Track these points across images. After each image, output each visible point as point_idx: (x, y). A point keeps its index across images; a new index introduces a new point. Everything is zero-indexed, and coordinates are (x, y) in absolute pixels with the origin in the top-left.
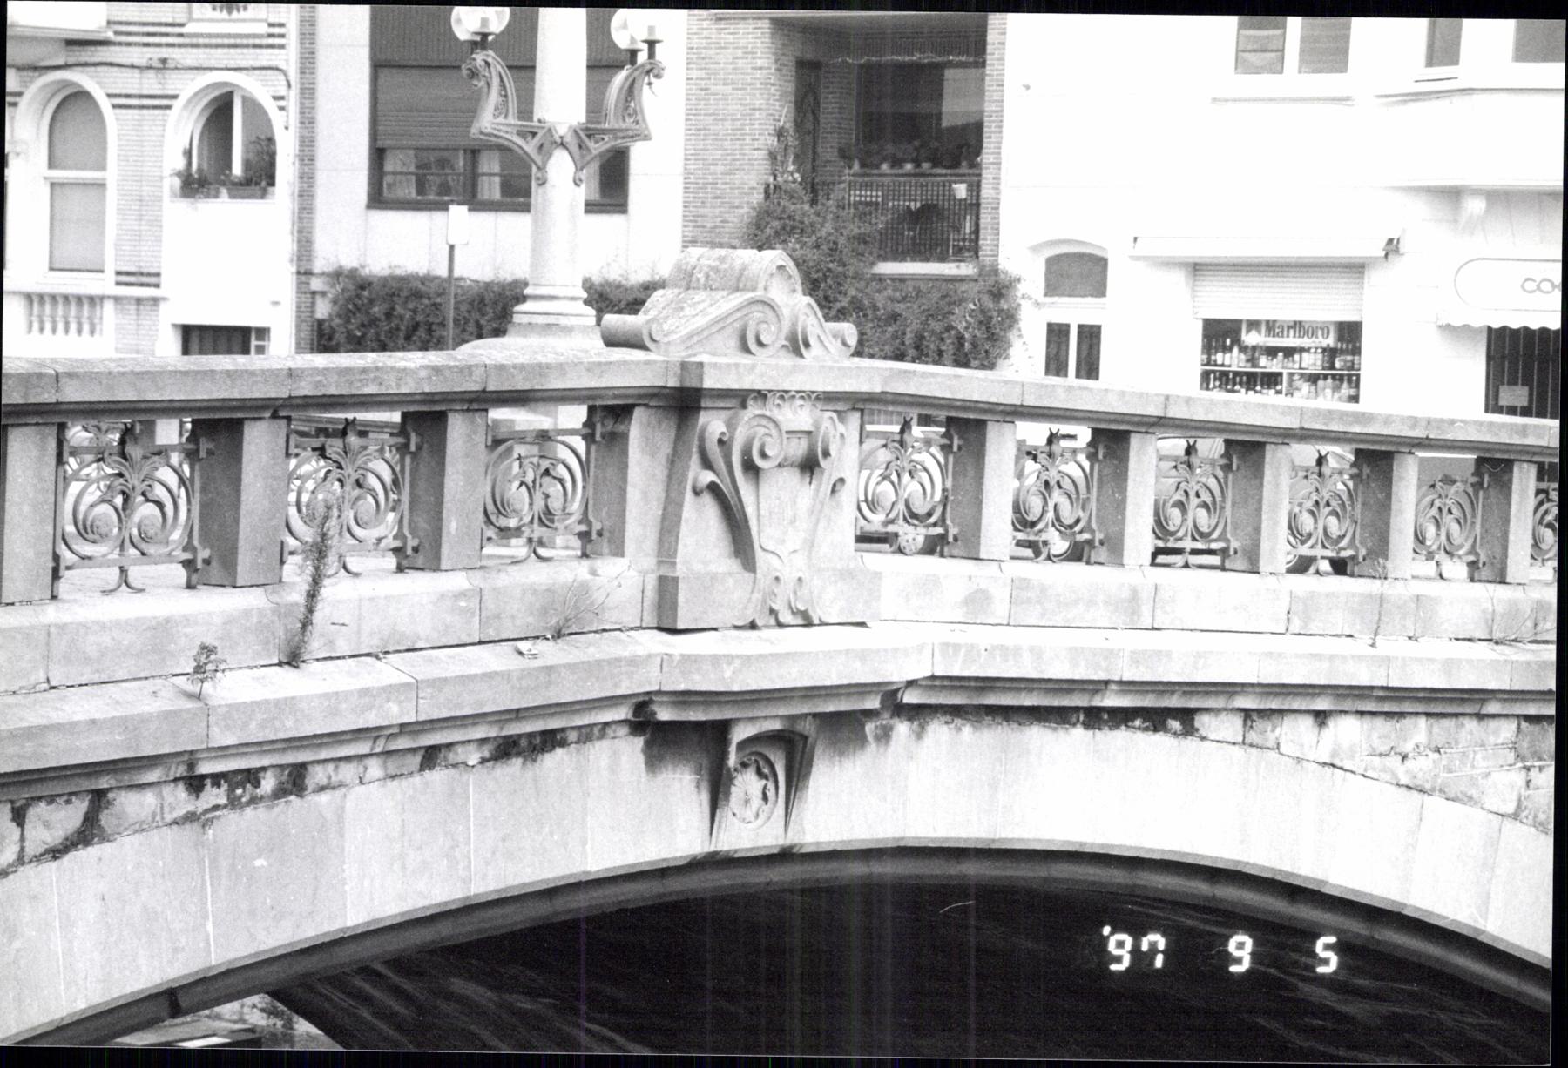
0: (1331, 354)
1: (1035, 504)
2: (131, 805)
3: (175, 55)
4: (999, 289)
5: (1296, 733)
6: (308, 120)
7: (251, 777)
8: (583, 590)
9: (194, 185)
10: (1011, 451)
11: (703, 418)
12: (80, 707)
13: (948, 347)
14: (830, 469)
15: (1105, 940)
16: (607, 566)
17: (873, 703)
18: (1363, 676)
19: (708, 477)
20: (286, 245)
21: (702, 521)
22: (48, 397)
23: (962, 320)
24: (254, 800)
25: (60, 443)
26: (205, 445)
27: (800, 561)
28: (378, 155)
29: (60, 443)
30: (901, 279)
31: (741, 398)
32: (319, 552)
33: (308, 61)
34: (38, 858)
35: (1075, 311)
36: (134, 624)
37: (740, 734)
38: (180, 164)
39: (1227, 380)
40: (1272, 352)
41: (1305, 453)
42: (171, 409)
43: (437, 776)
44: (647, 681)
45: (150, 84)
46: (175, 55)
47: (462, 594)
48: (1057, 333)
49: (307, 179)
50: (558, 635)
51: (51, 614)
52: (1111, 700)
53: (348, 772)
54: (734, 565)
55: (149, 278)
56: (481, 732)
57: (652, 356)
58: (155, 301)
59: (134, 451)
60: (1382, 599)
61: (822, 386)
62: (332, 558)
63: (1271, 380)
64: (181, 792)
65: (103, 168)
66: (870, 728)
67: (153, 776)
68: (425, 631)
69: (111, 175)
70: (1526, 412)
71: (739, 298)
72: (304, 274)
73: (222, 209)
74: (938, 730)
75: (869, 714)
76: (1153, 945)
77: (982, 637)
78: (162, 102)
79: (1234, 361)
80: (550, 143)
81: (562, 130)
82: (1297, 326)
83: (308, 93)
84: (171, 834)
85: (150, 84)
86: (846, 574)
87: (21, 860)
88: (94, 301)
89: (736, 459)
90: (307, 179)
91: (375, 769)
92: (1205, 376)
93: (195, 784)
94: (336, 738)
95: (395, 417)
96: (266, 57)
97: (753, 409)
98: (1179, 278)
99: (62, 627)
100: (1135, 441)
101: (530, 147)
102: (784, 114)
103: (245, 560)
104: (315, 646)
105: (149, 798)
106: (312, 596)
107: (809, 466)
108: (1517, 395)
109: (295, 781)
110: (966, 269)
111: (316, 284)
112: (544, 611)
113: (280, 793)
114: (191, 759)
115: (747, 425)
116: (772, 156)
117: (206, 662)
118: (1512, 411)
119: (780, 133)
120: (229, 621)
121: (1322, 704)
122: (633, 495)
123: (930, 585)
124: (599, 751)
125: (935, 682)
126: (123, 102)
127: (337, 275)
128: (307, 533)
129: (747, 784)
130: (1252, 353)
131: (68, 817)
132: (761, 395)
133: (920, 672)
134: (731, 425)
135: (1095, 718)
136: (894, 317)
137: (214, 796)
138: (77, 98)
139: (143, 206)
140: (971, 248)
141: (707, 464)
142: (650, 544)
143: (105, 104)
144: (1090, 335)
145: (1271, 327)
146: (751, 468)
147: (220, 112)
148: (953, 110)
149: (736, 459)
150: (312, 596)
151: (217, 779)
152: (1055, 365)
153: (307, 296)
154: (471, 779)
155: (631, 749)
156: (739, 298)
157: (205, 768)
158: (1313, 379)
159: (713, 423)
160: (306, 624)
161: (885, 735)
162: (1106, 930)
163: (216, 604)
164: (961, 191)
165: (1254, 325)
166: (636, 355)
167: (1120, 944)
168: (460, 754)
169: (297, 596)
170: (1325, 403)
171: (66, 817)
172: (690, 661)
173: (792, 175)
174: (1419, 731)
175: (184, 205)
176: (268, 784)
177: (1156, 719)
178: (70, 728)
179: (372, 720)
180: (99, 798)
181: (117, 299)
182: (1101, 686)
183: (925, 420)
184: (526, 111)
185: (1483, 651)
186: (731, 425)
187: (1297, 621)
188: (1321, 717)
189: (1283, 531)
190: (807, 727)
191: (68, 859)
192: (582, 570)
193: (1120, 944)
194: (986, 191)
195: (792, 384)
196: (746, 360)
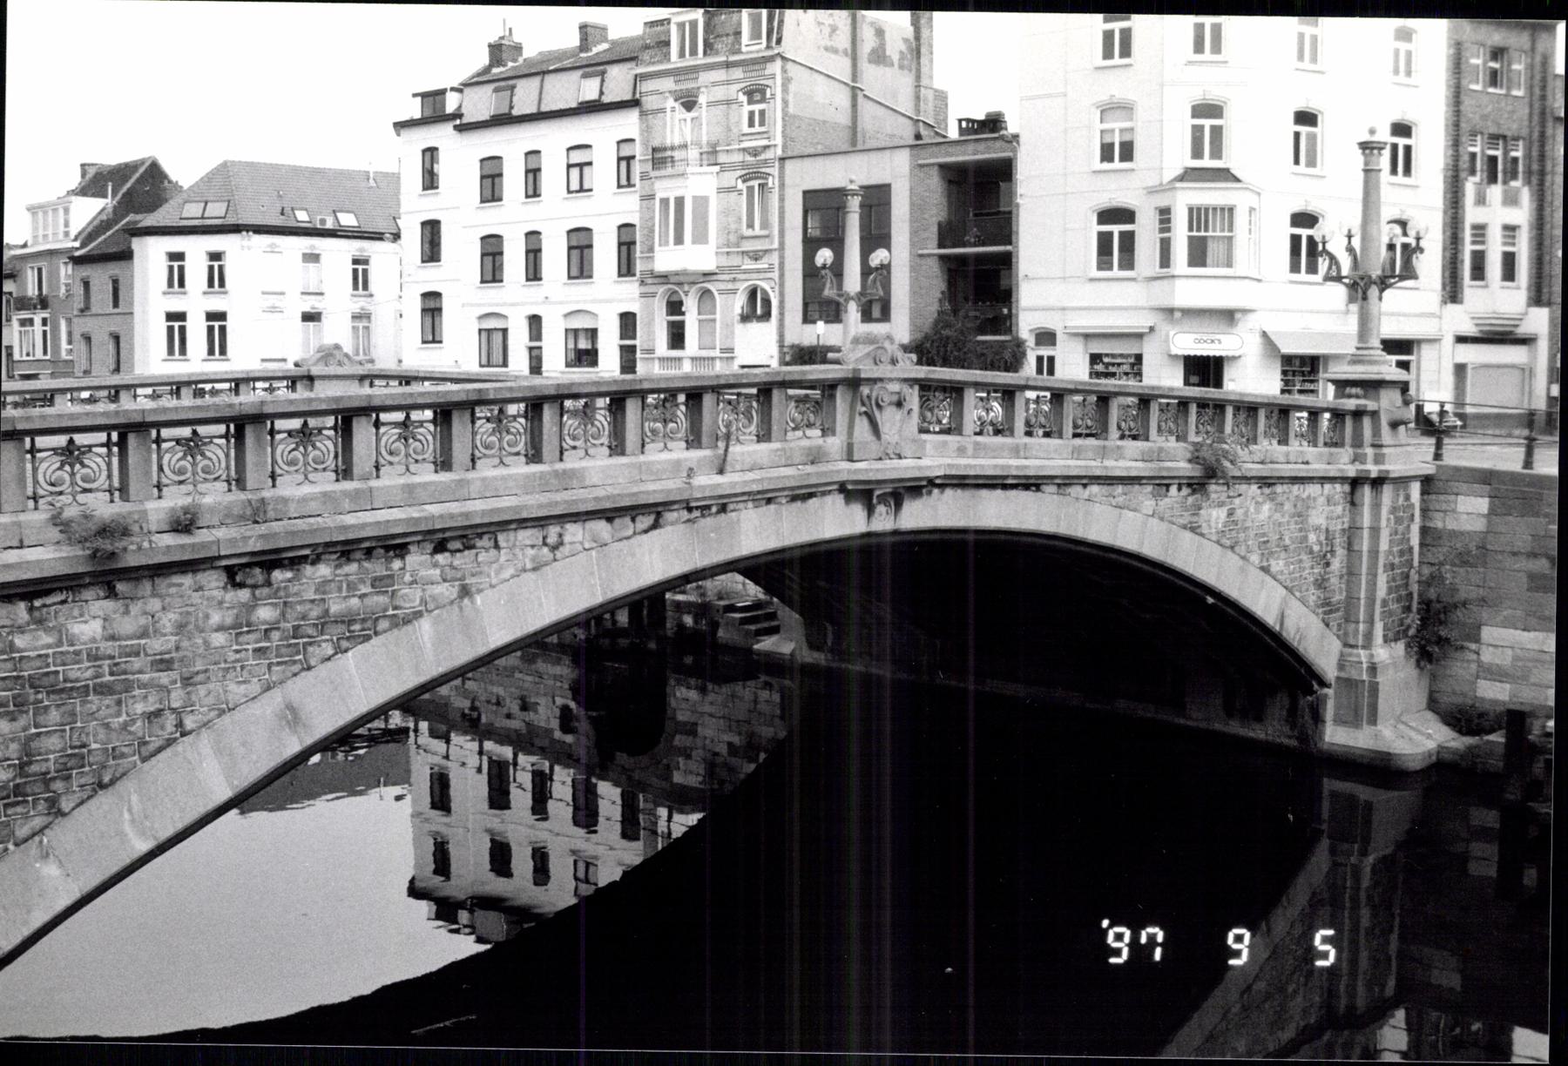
0: (1133, 365)
1: (1033, 420)
2: (670, 516)
3: (739, 276)
4: (1019, 344)
5: (1076, 490)
6: (782, 294)
7: (708, 507)
8: (820, 447)
9: (745, 318)
10: (1157, 407)
11: (862, 388)
12: (651, 487)
13: (1002, 364)
14: (907, 406)
15: (1105, 932)
16: (830, 440)
17: (924, 483)
18: (1098, 473)
19: (864, 409)
20: (774, 337)
21: (862, 425)
22: (638, 387)
23: (1007, 355)
24: (710, 515)
25: (643, 402)
26: (691, 402)
27: (896, 437)
28: (806, 305)
29: (643, 402)
30: (986, 342)
31: (874, 381)
32: (728, 437)
33: (782, 276)
34: (640, 533)
35: (1045, 352)
36: (668, 461)
37: (877, 493)
38: (740, 311)
39: (1098, 375)
40: (1113, 365)
41: (1078, 398)
42: (681, 390)
43: (772, 507)
44: (844, 477)
45: (730, 286)
46: (739, 276)
47: (778, 450)
48: (1040, 359)
49: (782, 314)
50: (813, 463)
51: (642, 458)
52: (1010, 481)
53: (741, 506)
54: (874, 438)
55: (731, 350)
56: (786, 493)
57: (844, 367)
58: (732, 358)
59: (668, 405)
60: (1104, 447)
61: (906, 376)
62: (733, 437)
63: (1113, 375)
64: (685, 512)
65: (714, 313)
66: (924, 491)
67: (676, 507)
68: (765, 461)
69: (718, 316)
70: (1198, 385)
71: (872, 347)
72: (781, 346)
73: (755, 327)
74: (949, 492)
75: (923, 487)
76: (1152, 938)
77: (963, 461)
78: (734, 292)
79: (1100, 368)
80: (848, 298)
81: (852, 294)
82: (1121, 356)
83: (782, 285)
84: (683, 526)
85: (730, 286)
86: (914, 441)
87: (635, 533)
88: (713, 359)
89: (873, 402)
90: (782, 314)
91: (750, 505)
92: (1091, 374)
93: (690, 509)
94: (736, 495)
95: (754, 391)
96: (769, 275)
97: (879, 385)
98: (1081, 339)
99: (645, 463)
100: (1018, 394)
101: (842, 300)
102: (943, 286)
103: (705, 440)
104: (728, 468)
105: (675, 514)
106: (726, 450)
107: (899, 404)
108: (1195, 379)
109: (723, 509)
110: (1007, 338)
111: (785, 350)
112: (808, 455)
113: (718, 512)
114: (687, 502)
115: (876, 390)
116: (940, 300)
117: (691, 472)
118: (1194, 385)
119: (943, 293)
120: (699, 461)
121: (1084, 481)
122: (839, 417)
123: (945, 443)
124: (828, 499)
125: (945, 477)
126: (721, 292)
127: (792, 346)
128: (724, 430)
129: (881, 509)
130: (1107, 365)
131: (649, 520)
132: (881, 380)
133: (941, 473)
134: (871, 390)
135: (1005, 487)
136: (983, 355)
137: (696, 513)
138: (707, 292)
139: (728, 327)
140: (1009, 331)
141: (863, 404)
142: (845, 432)
143: (716, 293)
144: (1051, 360)
145: (1113, 356)
146: (879, 407)
147: (753, 293)
148: (1004, 283)
149: (873, 402)
150: (726, 450)
151: (697, 508)
152: (1040, 371)
153: (782, 354)
154: (784, 508)
155: (839, 499)
156: (872, 347)
157: (693, 504)
158: (1126, 374)
159: (865, 390)
160: (724, 460)
161: (930, 493)
162: (1105, 923)
163: (696, 454)
164: (1005, 311)
165: (1107, 355)
166: (837, 367)
167: (1119, 937)
168: (779, 500)
169: (721, 451)
170: (1131, 383)
171: (645, 521)
172: (857, 471)
173: (947, 306)
174: (1119, 489)
175: (741, 325)
176: (714, 509)
177: (1027, 487)
178: (647, 493)
179: (747, 489)
180: (659, 514)
181: (721, 358)
182: (1006, 477)
183: (995, 391)
184: (840, 286)
185: (1140, 464)
186: (871, 390)
187: (1077, 453)
188: (1085, 486)
189: (1071, 425)
190: (902, 491)
191: (650, 534)
192: (821, 441)
193: (1119, 937)
194: (1014, 311)
195: (894, 375)
196: (875, 368)
